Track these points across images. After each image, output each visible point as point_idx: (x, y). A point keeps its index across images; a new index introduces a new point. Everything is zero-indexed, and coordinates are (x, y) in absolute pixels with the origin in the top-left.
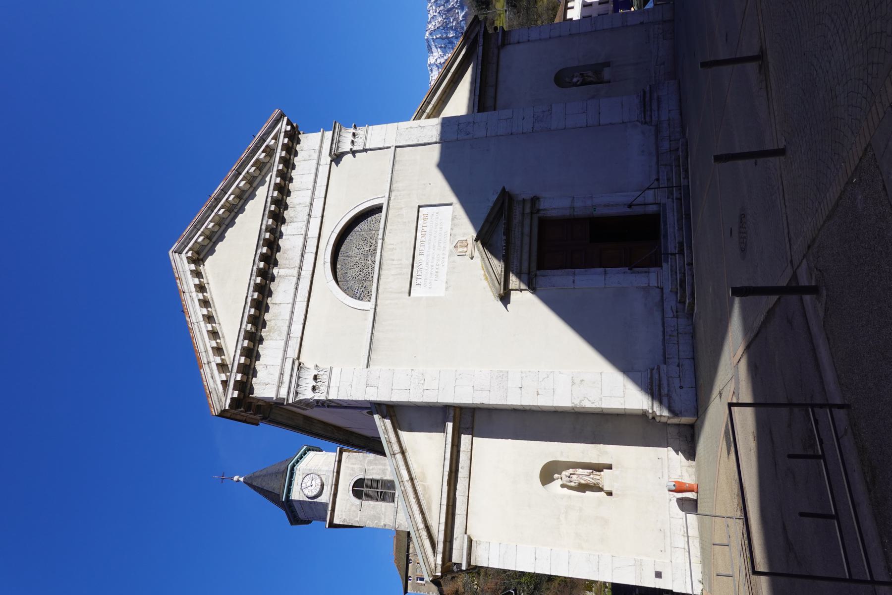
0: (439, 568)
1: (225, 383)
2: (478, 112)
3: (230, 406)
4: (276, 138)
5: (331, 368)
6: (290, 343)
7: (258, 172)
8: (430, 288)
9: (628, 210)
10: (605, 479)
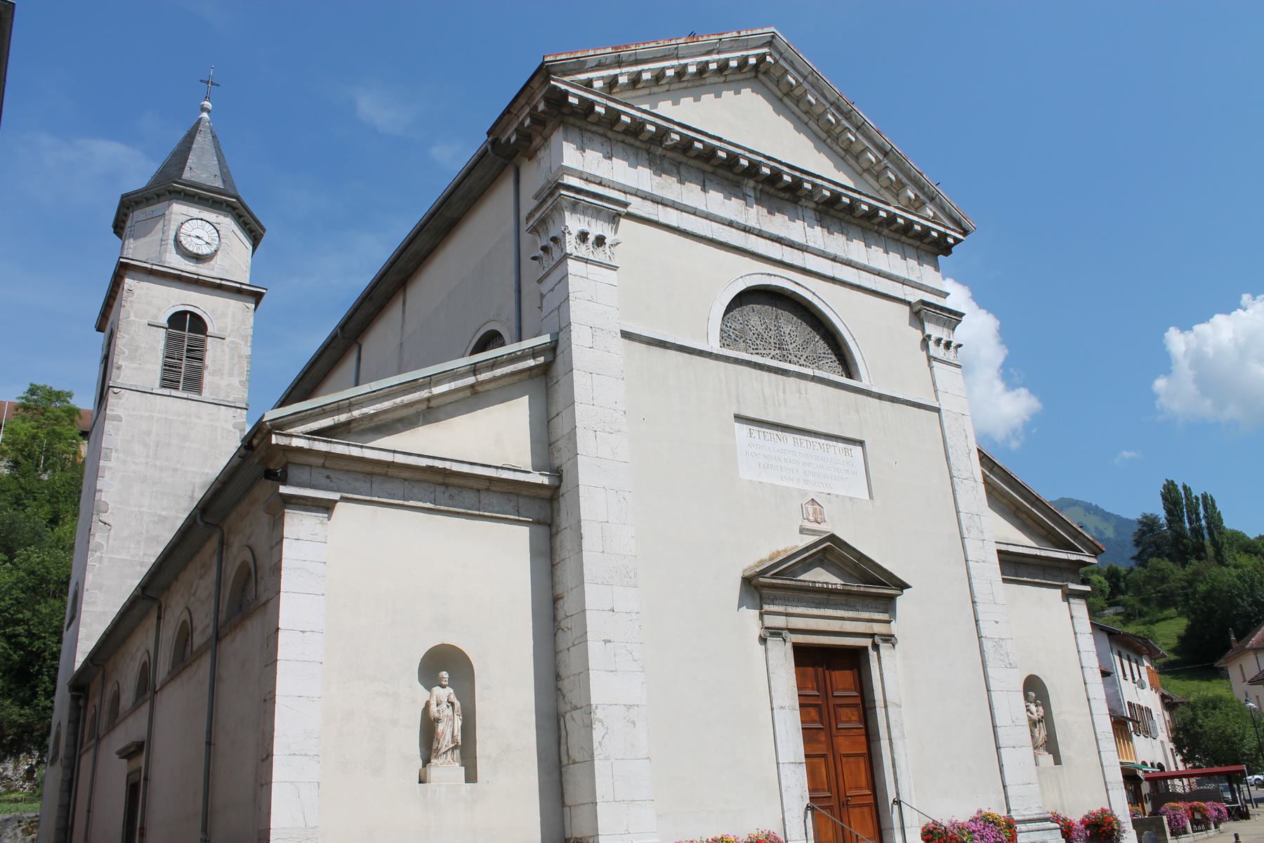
0: (283, 441)
1: (588, 84)
2: (999, 552)
3: (555, 87)
4: (934, 220)
5: (615, 268)
7: (886, 183)
9: (891, 801)
10: (447, 770)
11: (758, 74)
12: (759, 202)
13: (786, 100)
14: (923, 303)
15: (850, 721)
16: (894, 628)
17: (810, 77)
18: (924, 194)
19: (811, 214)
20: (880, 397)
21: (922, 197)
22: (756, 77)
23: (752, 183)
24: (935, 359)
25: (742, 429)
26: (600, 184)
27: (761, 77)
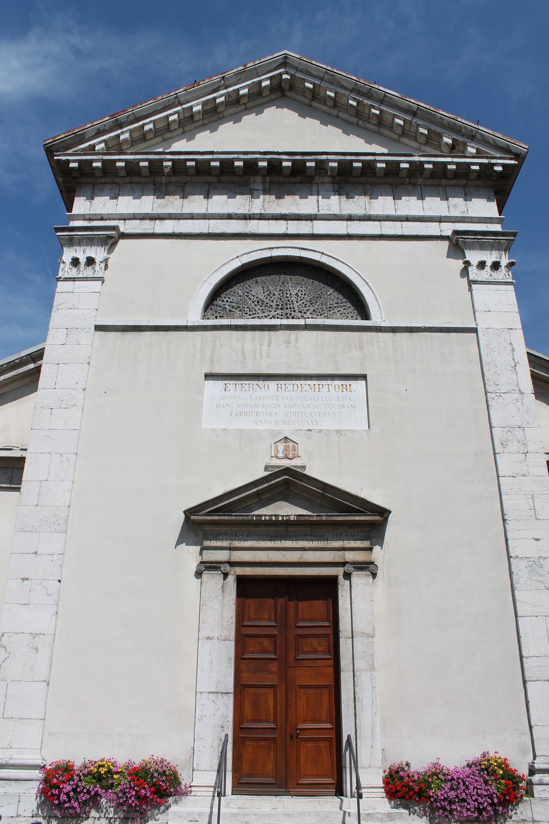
4: (479, 154)
6: (147, 222)
8: (218, 406)
11: (283, 93)
12: (266, 192)
13: (314, 104)
14: (456, 232)
15: (315, 652)
16: (378, 554)
17: (326, 77)
18: (463, 135)
19: (330, 187)
20: (394, 330)
21: (460, 139)
22: (283, 95)
23: (259, 179)
24: (475, 282)
25: (211, 383)
26: (102, 219)
27: (288, 94)
